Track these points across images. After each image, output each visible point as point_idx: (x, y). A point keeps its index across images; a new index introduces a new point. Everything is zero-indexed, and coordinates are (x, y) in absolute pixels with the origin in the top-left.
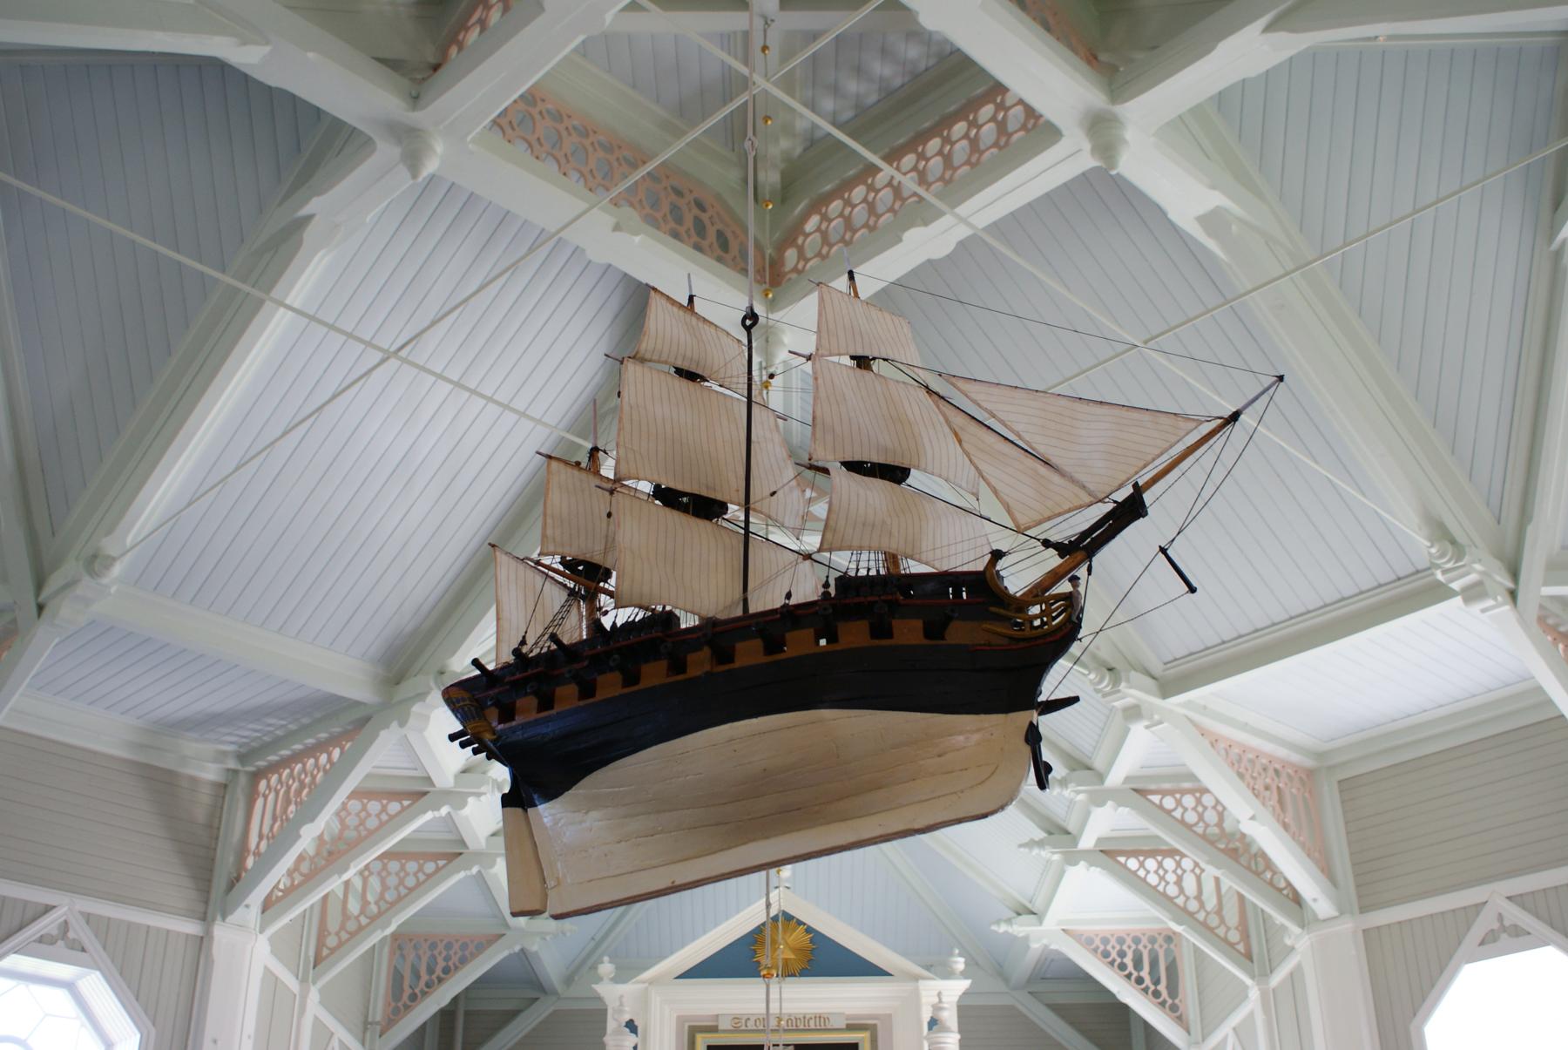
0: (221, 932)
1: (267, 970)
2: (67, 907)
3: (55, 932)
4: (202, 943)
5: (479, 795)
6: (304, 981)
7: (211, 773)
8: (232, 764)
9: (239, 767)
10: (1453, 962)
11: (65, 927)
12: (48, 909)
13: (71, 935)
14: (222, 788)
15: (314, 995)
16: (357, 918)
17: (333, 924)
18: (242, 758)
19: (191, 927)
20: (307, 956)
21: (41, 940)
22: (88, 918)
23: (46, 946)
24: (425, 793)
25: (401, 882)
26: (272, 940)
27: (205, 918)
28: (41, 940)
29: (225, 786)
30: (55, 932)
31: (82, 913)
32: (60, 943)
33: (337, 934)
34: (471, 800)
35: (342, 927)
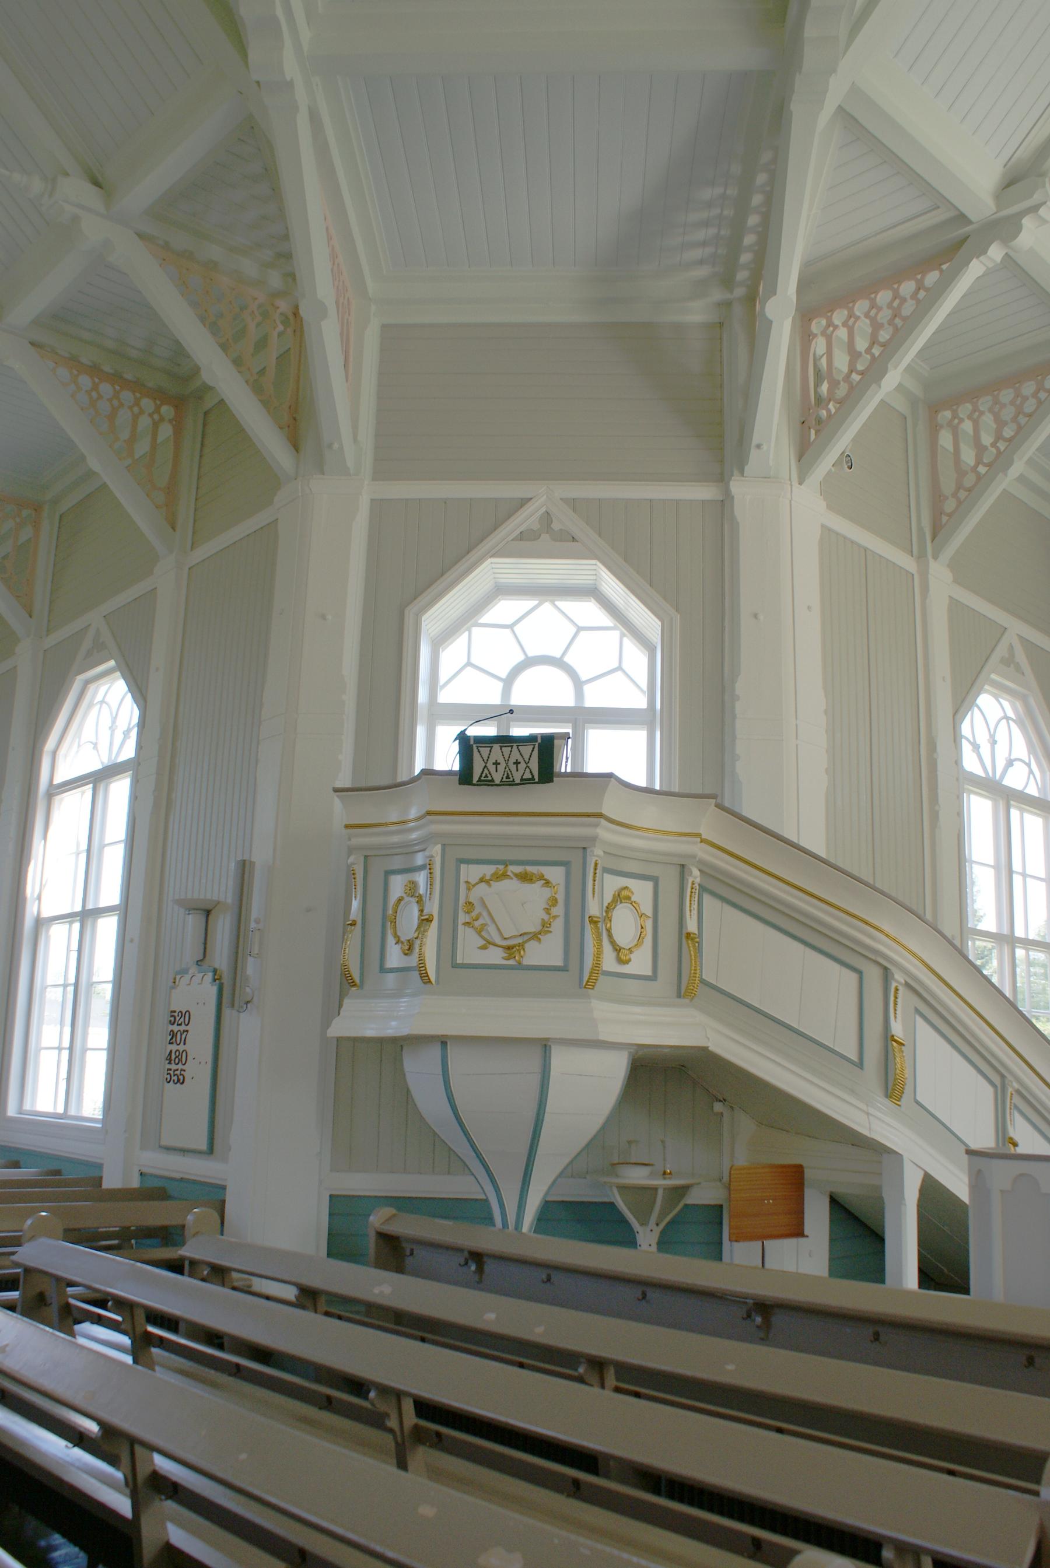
0: (736, 486)
1: (826, 530)
2: (544, 497)
3: (536, 527)
4: (724, 506)
5: (1035, 209)
6: (921, 557)
7: (697, 313)
8: (717, 295)
9: (728, 296)
10: (24, 1141)
11: (547, 518)
12: (524, 502)
13: (556, 526)
14: (718, 328)
15: (940, 573)
16: (974, 469)
17: (948, 485)
18: (727, 281)
19: (704, 492)
20: (920, 529)
21: (522, 537)
22: (574, 504)
23: (531, 542)
24: (963, 240)
25: (1019, 411)
26: (828, 490)
27: (722, 479)
28: (522, 537)
29: (721, 324)
30: (536, 527)
31: (564, 500)
32: (545, 537)
33: (955, 495)
34: (1027, 222)
35: (959, 486)
